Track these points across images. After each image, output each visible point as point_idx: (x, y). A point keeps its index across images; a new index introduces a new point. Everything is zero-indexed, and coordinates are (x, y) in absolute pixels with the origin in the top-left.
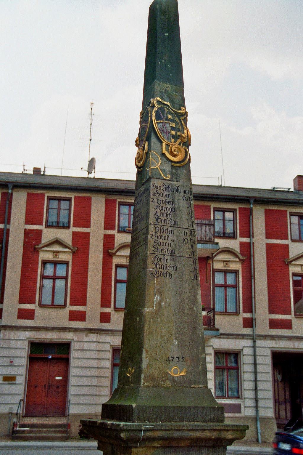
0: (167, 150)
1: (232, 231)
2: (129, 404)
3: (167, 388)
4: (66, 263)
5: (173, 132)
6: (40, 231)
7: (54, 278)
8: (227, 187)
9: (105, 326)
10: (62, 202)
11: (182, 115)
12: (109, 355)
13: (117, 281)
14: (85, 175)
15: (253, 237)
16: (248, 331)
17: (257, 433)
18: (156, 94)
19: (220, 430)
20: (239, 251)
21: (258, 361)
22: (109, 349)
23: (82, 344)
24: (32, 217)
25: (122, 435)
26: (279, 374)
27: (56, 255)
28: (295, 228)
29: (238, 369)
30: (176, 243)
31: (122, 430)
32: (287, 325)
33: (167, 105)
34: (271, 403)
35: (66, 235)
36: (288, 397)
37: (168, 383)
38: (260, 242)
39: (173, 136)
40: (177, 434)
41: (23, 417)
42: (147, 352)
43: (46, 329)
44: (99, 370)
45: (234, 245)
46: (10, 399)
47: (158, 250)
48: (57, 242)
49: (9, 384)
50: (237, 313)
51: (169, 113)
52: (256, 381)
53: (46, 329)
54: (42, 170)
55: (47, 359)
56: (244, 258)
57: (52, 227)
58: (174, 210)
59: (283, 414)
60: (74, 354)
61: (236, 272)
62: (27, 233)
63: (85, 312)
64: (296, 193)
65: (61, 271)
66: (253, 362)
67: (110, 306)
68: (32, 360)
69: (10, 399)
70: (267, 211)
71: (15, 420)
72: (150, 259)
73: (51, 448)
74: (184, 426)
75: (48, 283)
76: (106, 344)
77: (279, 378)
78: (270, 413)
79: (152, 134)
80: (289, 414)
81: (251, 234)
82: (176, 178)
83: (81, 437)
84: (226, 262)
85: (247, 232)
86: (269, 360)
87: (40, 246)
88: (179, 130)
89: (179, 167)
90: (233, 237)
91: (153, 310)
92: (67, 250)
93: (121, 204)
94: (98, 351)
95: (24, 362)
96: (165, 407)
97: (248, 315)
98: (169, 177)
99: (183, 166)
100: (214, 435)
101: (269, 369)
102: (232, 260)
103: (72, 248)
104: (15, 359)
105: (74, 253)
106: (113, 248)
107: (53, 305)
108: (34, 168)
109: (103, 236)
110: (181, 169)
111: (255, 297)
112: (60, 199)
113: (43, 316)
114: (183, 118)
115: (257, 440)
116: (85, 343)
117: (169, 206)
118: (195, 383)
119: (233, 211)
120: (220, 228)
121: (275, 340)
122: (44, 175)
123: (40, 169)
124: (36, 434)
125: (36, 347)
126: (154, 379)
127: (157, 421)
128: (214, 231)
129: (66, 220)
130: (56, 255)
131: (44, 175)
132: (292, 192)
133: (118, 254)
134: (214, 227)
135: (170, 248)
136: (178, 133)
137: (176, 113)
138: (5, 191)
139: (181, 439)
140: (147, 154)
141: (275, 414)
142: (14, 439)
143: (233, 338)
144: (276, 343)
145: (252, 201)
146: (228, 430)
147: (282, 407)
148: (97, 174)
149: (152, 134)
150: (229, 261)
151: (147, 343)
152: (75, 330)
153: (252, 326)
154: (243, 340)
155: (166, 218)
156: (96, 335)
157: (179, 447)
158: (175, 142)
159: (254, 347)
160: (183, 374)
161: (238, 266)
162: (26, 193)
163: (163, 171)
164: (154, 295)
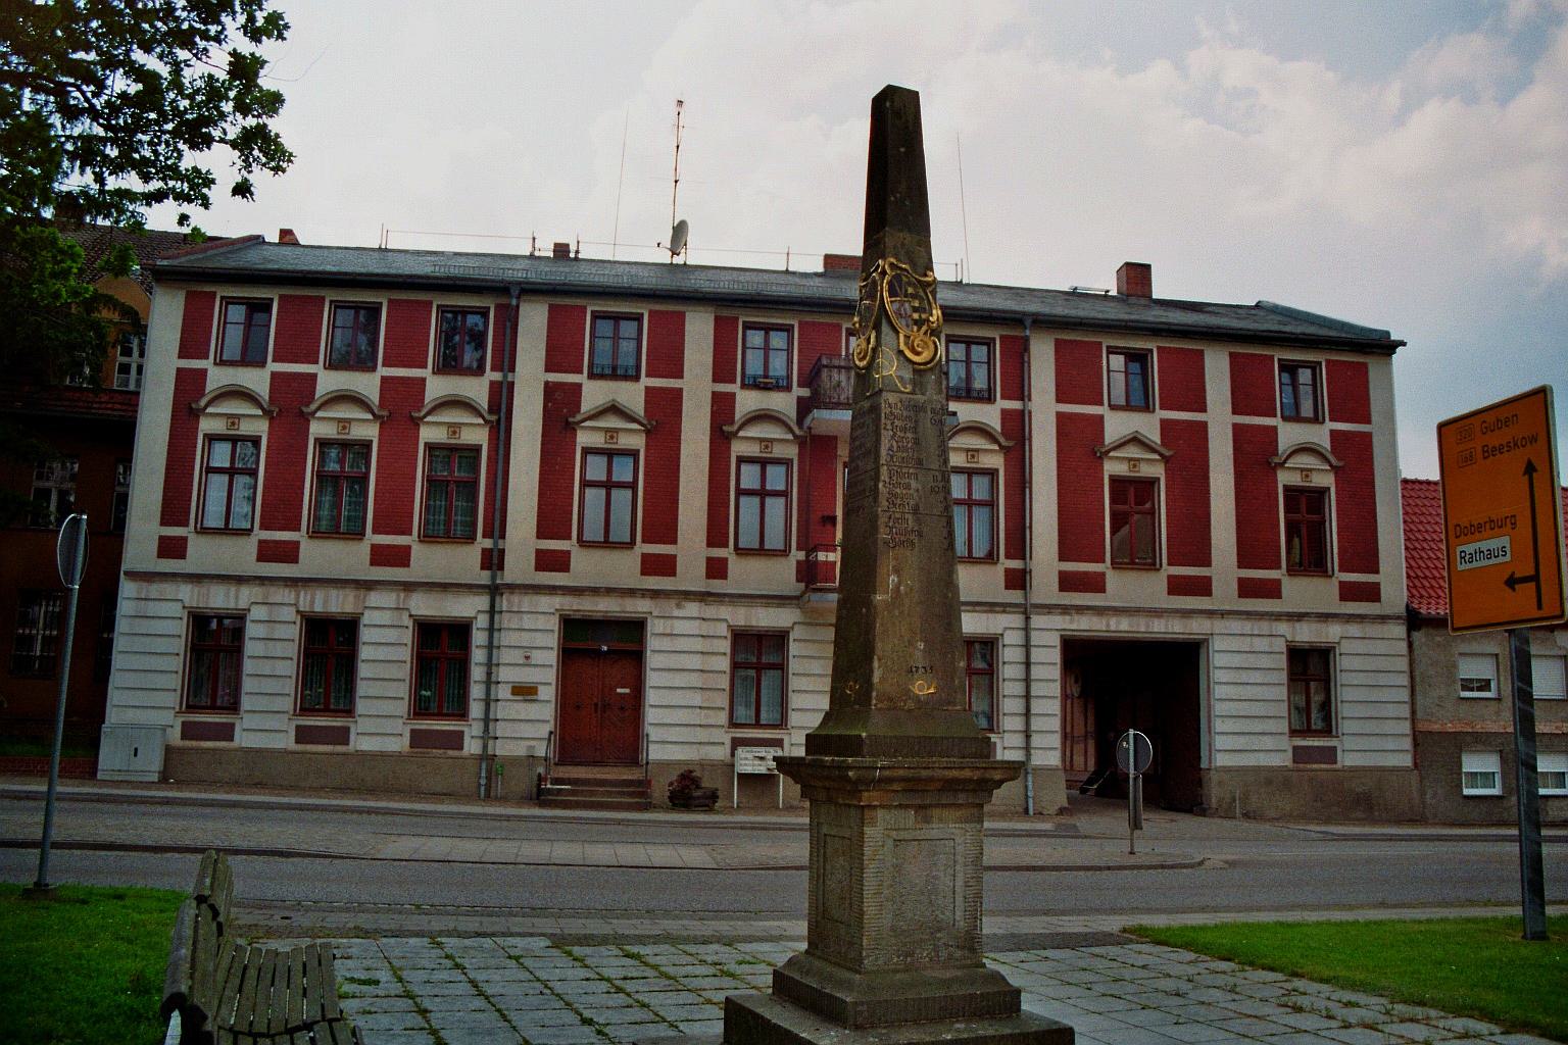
0: (906, 344)
1: (985, 387)
2: (855, 732)
3: (909, 711)
4: (633, 454)
5: (916, 316)
6: (579, 386)
7: (609, 485)
8: (973, 285)
9: (717, 586)
10: (623, 324)
11: (929, 284)
12: (725, 646)
13: (740, 492)
14: (664, 257)
15: (1030, 400)
16: (1016, 596)
17: (1027, 796)
18: (888, 250)
19: (985, 768)
20: (998, 427)
21: (1034, 658)
22: (725, 634)
23: (669, 622)
24: (560, 355)
25: (850, 774)
26: (1076, 682)
27: (612, 437)
28: (1119, 380)
29: (992, 674)
30: (921, 492)
31: (850, 768)
32: (1096, 584)
33: (905, 270)
34: (1055, 740)
35: (632, 395)
36: (1091, 728)
37: (911, 705)
38: (1044, 409)
39: (916, 322)
40: (924, 773)
41: (556, 764)
42: (879, 660)
43: (595, 591)
44: (705, 675)
45: (990, 415)
46: (528, 731)
47: (894, 505)
48: (614, 409)
49: (526, 700)
50: (991, 558)
51: (909, 284)
52: (1027, 697)
53: (595, 591)
54: (573, 248)
55: (599, 653)
56: (1340, 464)
57: (602, 377)
58: (917, 442)
59: (1079, 760)
60: (652, 643)
61: (992, 473)
62: (550, 390)
63: (675, 556)
64: (1124, 301)
65: (623, 471)
66: (1024, 660)
67: (726, 545)
68: (569, 655)
69: (528, 731)
70: (1059, 344)
71: (541, 770)
72: (882, 520)
73: (619, 822)
74: (934, 762)
75: (750, 505)
76: (718, 624)
77: (1076, 690)
78: (1053, 759)
79: (884, 321)
80: (1091, 763)
81: (1026, 393)
82: (921, 390)
83: (674, 805)
84: (973, 453)
85: (1018, 387)
86: (1056, 656)
87: (579, 417)
88: (924, 311)
89: (924, 371)
90: (366, 364)
91: (887, 597)
92: (635, 426)
93: (748, 326)
94: (702, 636)
95: (552, 657)
96: (908, 737)
97: (1016, 564)
98: (909, 389)
99: (931, 369)
100: (976, 775)
101: (1056, 673)
102: (983, 447)
103: (645, 422)
104: (534, 651)
105: (648, 432)
106: (732, 422)
107: (607, 541)
108: (556, 245)
109: (709, 396)
110: (929, 374)
111: (1031, 527)
112: (617, 318)
113: (586, 566)
114: (930, 289)
115: (1026, 811)
116: (675, 621)
117: (910, 435)
118: (949, 703)
119: (988, 343)
120: (960, 378)
121: (1069, 614)
122: (576, 259)
123: (568, 245)
124: (580, 796)
125: (572, 626)
126: (891, 700)
127: (896, 757)
128: (948, 387)
129: (632, 362)
130: (612, 437)
131: (576, 259)
132: (1113, 297)
133: (741, 434)
134: (948, 379)
135: (912, 502)
136: (924, 316)
137: (919, 281)
138: (503, 300)
139: (931, 779)
140: (874, 350)
141: (1064, 760)
142: (543, 804)
143: (985, 612)
144: (1071, 622)
145: (1028, 322)
146: (995, 768)
147: (1079, 748)
148: (693, 255)
149: (884, 321)
150: (977, 450)
151: (879, 645)
152: (655, 594)
153: (1023, 587)
154: (1004, 615)
155: (905, 455)
156: (697, 604)
157: (927, 791)
158: (918, 330)
159: (1027, 629)
160: (932, 691)
161: (996, 461)
162: (546, 307)
163: (901, 378)
164: (889, 576)
